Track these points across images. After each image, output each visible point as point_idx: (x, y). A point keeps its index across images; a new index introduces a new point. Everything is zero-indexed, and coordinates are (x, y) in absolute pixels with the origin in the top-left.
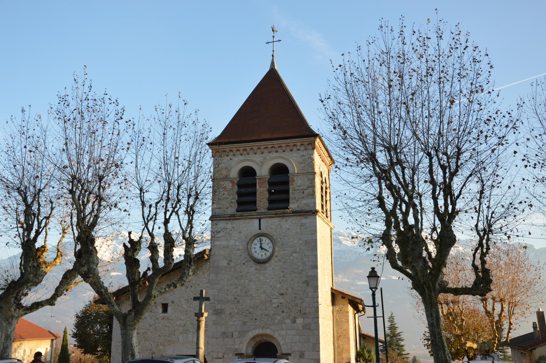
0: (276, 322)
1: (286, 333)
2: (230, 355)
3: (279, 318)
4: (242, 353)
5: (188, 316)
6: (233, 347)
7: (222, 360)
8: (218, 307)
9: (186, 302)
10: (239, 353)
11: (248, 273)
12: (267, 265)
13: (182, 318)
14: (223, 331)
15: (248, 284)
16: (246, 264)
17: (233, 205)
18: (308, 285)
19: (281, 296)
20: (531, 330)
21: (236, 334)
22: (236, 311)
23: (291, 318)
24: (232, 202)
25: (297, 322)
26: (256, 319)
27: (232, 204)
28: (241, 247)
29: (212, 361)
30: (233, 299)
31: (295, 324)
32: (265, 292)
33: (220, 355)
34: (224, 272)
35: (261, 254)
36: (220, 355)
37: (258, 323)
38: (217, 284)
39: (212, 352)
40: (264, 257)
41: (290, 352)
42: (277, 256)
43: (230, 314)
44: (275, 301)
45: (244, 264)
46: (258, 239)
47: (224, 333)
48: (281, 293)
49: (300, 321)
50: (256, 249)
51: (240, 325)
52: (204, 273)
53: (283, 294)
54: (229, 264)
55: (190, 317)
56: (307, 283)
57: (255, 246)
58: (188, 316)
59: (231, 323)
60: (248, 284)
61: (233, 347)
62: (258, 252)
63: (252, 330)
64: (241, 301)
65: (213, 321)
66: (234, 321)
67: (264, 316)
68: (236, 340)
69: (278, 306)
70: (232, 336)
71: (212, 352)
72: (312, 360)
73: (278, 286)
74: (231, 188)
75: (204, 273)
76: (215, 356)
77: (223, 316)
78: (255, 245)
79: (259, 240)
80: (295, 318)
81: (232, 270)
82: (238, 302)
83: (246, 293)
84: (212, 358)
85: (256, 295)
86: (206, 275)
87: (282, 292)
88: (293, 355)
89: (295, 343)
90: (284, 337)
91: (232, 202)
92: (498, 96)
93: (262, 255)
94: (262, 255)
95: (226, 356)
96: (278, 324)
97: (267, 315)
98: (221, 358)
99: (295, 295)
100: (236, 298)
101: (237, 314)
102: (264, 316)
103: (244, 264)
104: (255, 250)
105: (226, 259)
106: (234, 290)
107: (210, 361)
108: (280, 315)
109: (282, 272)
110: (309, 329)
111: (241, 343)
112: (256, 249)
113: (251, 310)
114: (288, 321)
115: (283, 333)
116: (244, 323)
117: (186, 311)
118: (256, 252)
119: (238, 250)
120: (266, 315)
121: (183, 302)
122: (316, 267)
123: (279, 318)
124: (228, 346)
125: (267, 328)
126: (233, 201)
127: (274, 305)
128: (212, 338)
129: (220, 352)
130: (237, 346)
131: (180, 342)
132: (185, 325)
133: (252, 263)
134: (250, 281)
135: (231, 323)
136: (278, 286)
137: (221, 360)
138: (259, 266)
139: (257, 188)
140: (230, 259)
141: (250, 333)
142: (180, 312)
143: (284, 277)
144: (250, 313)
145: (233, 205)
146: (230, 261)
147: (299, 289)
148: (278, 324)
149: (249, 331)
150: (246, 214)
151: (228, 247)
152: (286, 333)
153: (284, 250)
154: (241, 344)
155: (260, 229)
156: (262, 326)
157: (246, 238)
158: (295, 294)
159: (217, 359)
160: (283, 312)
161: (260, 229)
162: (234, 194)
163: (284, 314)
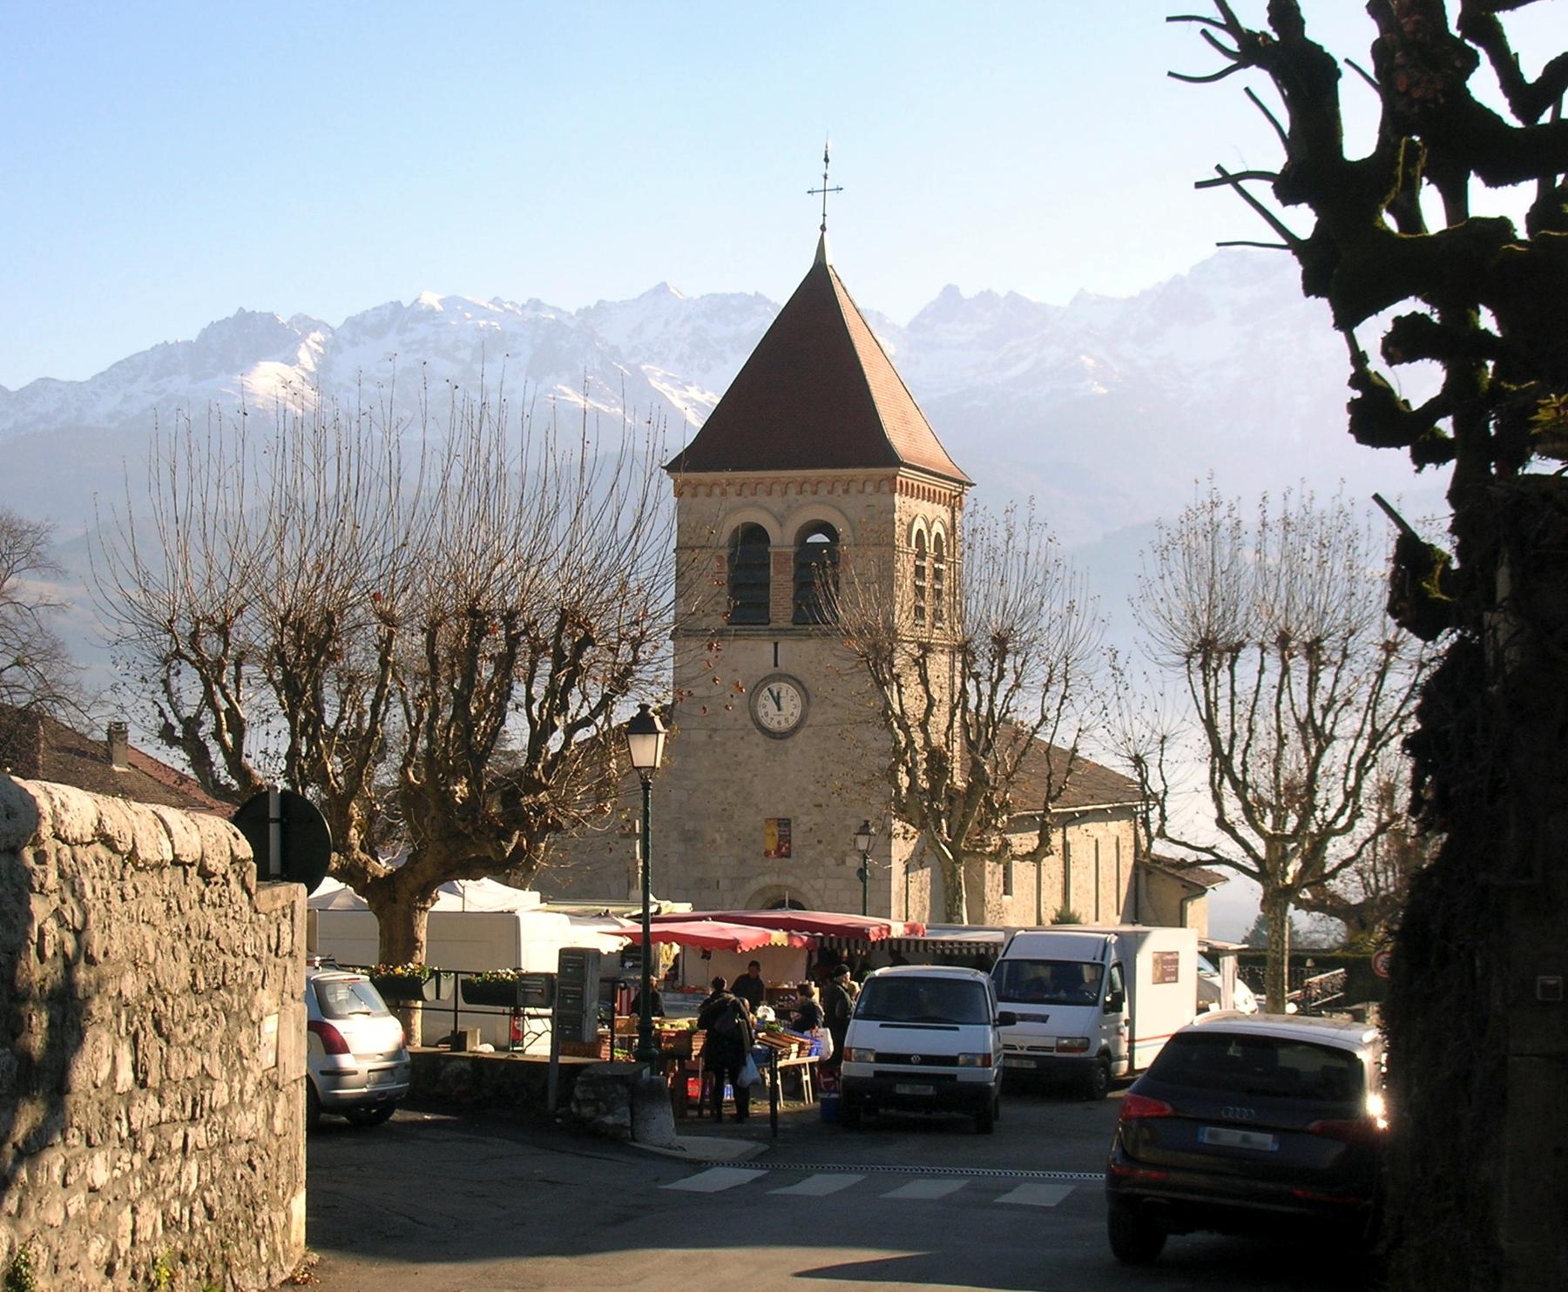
0: (806, 862)
3: (811, 853)
8: (690, 825)
12: (789, 743)
15: (751, 782)
45: (742, 738)
60: (751, 782)
62: (770, 715)
64: (736, 817)
69: (811, 829)
73: (812, 788)
80: (845, 854)
82: (731, 817)
87: (820, 800)
93: (779, 723)
94: (779, 723)
100: (725, 810)
114: (830, 862)
115: (819, 884)
116: (743, 862)
123: (811, 853)
133: (758, 736)
134: (756, 775)
138: (773, 743)
141: (753, 882)
149: (752, 878)
160: (819, 842)
161: (776, 665)
163: (821, 847)
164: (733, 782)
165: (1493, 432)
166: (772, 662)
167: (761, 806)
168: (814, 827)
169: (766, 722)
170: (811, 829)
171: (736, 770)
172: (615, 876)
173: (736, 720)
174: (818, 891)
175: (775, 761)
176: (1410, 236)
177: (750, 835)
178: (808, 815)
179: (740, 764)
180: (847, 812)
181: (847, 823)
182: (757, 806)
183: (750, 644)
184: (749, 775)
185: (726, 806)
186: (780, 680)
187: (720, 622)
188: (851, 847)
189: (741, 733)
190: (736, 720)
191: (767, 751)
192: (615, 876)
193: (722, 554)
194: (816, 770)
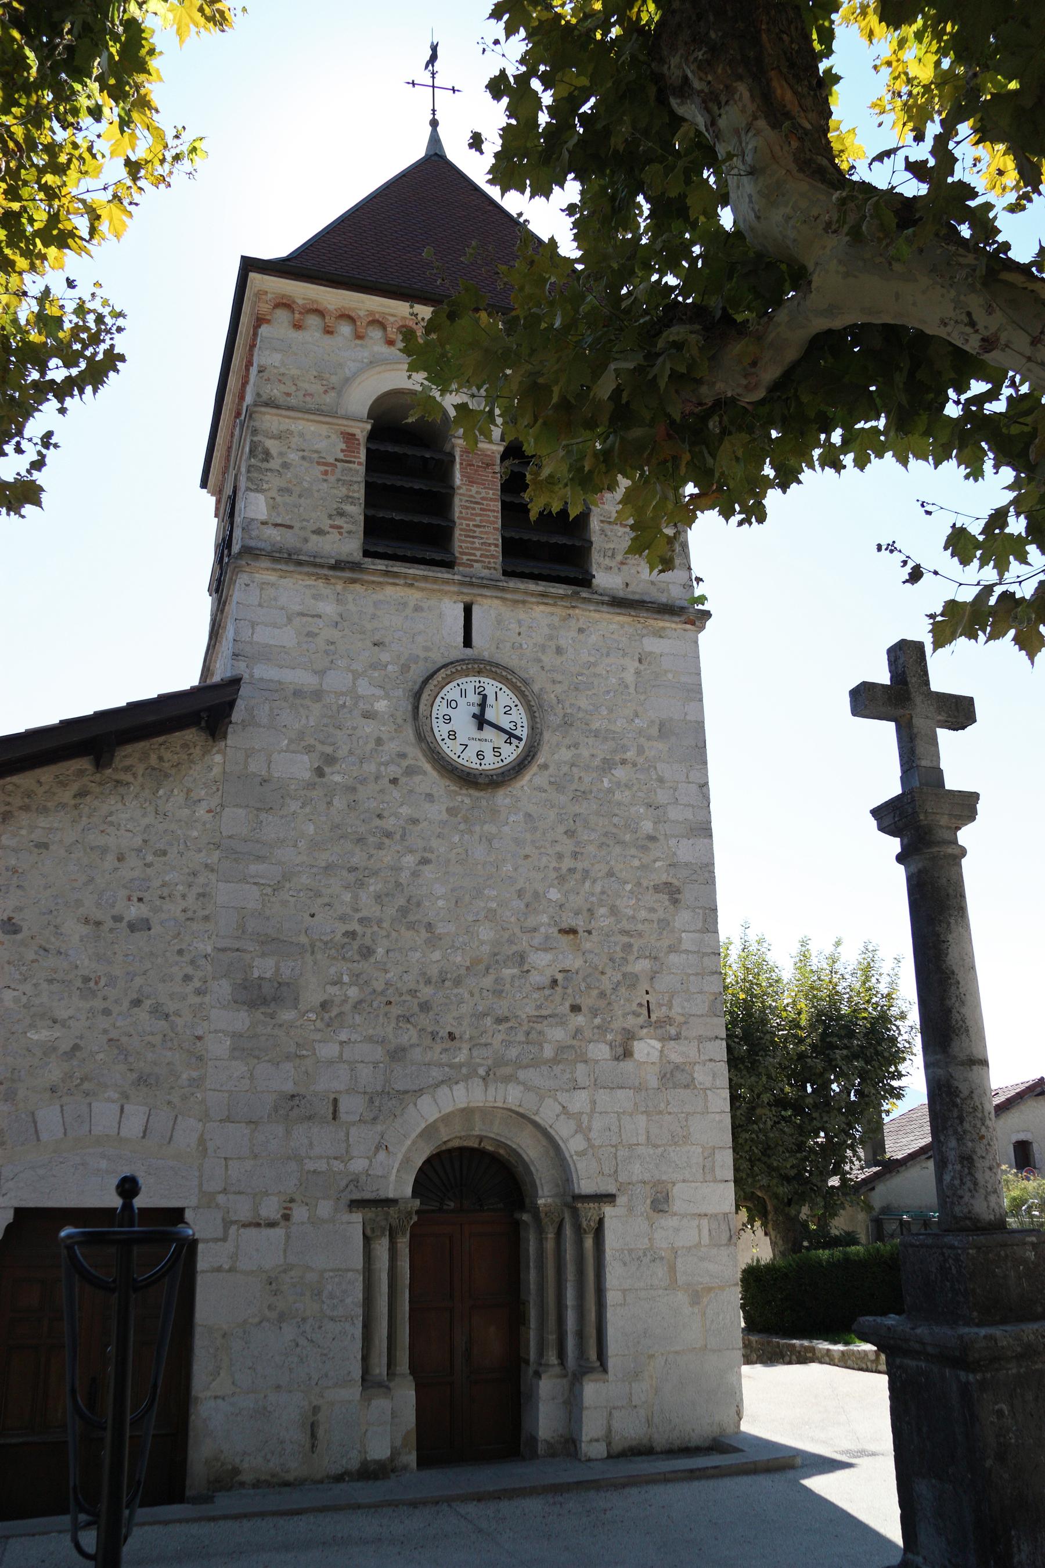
0: (548, 1052)
1: (594, 1103)
2: (325, 1209)
3: (557, 1034)
4: (383, 1195)
5: (98, 1004)
6: (338, 1166)
7: (278, 1233)
8: (264, 967)
9: (85, 930)
10: (367, 1196)
11: (415, 821)
12: (502, 798)
13: (62, 1014)
14: (289, 1087)
15: (415, 874)
16: (403, 780)
17: (347, 527)
18: (675, 902)
19: (565, 939)
20: (951, 783)
21: (352, 1106)
22: (353, 992)
23: (609, 1037)
24: (341, 514)
25: (636, 1056)
26: (451, 1036)
27: (339, 521)
28: (381, 706)
29: (224, 1239)
30: (338, 937)
31: (627, 1065)
32: (491, 915)
33: (271, 1209)
34: (294, 806)
35: (474, 747)
36: (271, 1209)
37: (462, 1057)
38: (260, 859)
39: (224, 1191)
40: (490, 763)
41: (612, 1189)
42: (545, 767)
43: (324, 1005)
44: (540, 960)
45: (394, 781)
46: (523, 732)
47: (293, 1096)
48: (564, 925)
49: (647, 1049)
50: (453, 726)
51: (376, 1065)
52: (192, 802)
53: (572, 931)
54: (320, 772)
55: (107, 1012)
56: (672, 893)
57: (449, 711)
58: (98, 1004)
59: (328, 1050)
60: (415, 874)
61: (338, 1166)
62: (461, 738)
63: (437, 1086)
64: (380, 951)
65: (236, 1036)
66: (342, 1043)
67: (489, 1021)
68: (353, 1131)
69: (555, 982)
70: (334, 1118)
71: (224, 1191)
72: (705, 1222)
73: (554, 894)
74: (341, 456)
75: (192, 802)
76: (243, 1210)
77: (287, 1015)
78: (449, 704)
79: (517, 733)
80: (629, 1036)
81: (336, 801)
82: (367, 952)
83: (404, 911)
84: (227, 1224)
85: (451, 928)
86: (201, 812)
87: (568, 920)
88: (621, 1200)
89: (630, 1146)
90: (585, 1119)
91: (341, 514)
92: (503, 55)
93: (480, 754)
94: (480, 754)
95: (299, 1213)
96: (555, 1061)
97: (506, 1019)
98: (272, 1225)
99: (626, 939)
100: (352, 935)
101: (357, 1006)
102: (489, 1021)
103: (394, 781)
104: (449, 727)
105: (309, 749)
106: (347, 897)
107: (216, 1240)
108: (563, 1023)
109: (570, 833)
110: (687, 1086)
111: (378, 1148)
112: (453, 726)
113: (426, 992)
114: (600, 1051)
115: (579, 1101)
116: (397, 1054)
117: (86, 980)
118: (452, 735)
119: (368, 715)
120: (499, 1021)
121: (74, 930)
122: (704, 830)
123: (557, 1034)
124: (310, 1166)
125: (507, 1079)
126: (349, 508)
127: (535, 978)
128: (228, 1119)
129: (266, 1194)
130: (358, 1165)
131: (44, 1136)
132: (76, 1047)
133: (431, 779)
134: (425, 861)
135: (328, 1050)
136: (554, 894)
137: (271, 1232)
138: (465, 798)
139: (458, 479)
140: (329, 750)
141: (425, 1103)
142: (50, 981)
143: (575, 855)
144: (425, 1007)
145: (347, 527)
146: (330, 760)
147: (643, 914)
148: (555, 1061)
149: (420, 1092)
150: (398, 567)
151: (317, 695)
152: (594, 1103)
153: (576, 745)
154: (382, 1155)
155: (468, 642)
156: (482, 1071)
157: (405, 668)
158: (624, 932)
159: (253, 1231)
160: (576, 1009)
161: (468, 642)
162: (351, 483)
163: (580, 1020)
164: (375, 873)
165: (63, 1234)
166: (461, 639)
167: (441, 929)
168: (560, 977)
169: (450, 749)
170: (555, 982)
171: (380, 847)
172: (53, 1090)
173: (379, 741)
174: (577, 1117)
175: (471, 832)
176: (165, 1228)
177: (413, 993)
178: (546, 950)
179: (389, 835)
180: (630, 945)
181: (629, 969)
182: (429, 926)
183: (413, 596)
184: (409, 860)
185: (355, 926)
186: (479, 673)
187: (351, 546)
188: (641, 1020)
189: (393, 770)
190: (379, 741)
191: (451, 811)
192: (53, 1090)
193: (357, 432)
194: (560, 856)
